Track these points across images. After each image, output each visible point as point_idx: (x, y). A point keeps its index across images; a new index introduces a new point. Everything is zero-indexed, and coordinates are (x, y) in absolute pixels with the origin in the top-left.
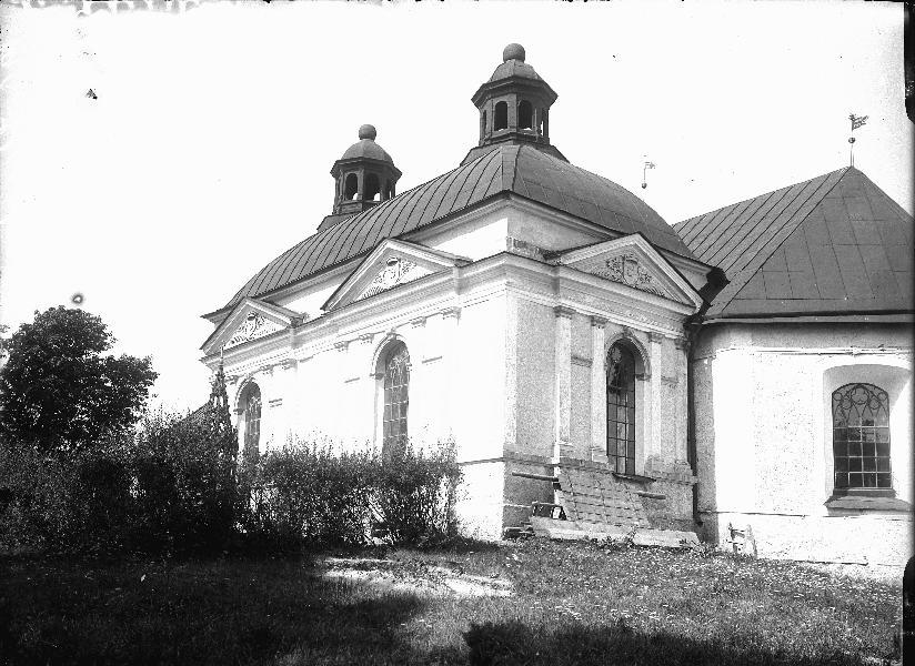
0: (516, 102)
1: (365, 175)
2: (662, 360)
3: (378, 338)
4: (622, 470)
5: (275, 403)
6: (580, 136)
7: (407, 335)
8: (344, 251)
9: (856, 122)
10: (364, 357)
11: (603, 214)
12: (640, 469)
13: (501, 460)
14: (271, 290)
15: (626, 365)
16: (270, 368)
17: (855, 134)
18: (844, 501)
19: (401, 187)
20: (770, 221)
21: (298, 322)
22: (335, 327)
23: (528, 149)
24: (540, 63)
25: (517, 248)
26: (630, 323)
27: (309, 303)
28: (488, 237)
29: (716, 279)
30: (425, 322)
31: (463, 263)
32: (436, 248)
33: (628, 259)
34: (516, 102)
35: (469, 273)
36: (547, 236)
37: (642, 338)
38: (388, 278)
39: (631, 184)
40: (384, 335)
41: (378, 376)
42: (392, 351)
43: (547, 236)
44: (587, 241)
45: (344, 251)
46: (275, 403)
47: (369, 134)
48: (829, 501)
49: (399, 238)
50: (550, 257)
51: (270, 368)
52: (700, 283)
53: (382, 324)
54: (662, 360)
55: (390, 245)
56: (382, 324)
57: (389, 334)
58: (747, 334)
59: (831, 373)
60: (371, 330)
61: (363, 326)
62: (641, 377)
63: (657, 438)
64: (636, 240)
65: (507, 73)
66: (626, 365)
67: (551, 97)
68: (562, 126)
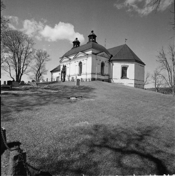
2: (106, 64)
3: (79, 61)
5: (68, 68)
6: (100, 41)
7: (82, 62)
8: (87, 48)
10: (77, 64)
11: (102, 50)
12: (104, 75)
15: (103, 65)
16: (83, 60)
19: (80, 45)
23: (94, 43)
24: (95, 33)
27: (72, 57)
28: (90, 52)
29: (112, 56)
31: (87, 55)
33: (103, 54)
34: (93, 37)
36: (96, 52)
38: (80, 56)
39: (104, 46)
42: (80, 64)
45: (87, 48)
46: (68, 68)
47: (77, 39)
49: (81, 51)
50: (96, 54)
51: (67, 64)
53: (81, 60)
55: (80, 52)
56: (79, 61)
59: (121, 66)
61: (78, 60)
63: (106, 72)
64: (104, 53)
65: (76, 41)
66: (103, 65)
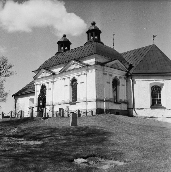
0: (94, 33)
1: (64, 44)
2: (122, 82)
3: (71, 78)
4: (115, 102)
6: (106, 40)
9: (154, 36)
10: (68, 82)
12: (118, 101)
13: (69, 103)
14: (47, 67)
15: (115, 83)
17: (154, 38)
18: (153, 106)
19: (72, 47)
20: (137, 61)
21: (54, 74)
22: (62, 76)
24: (98, 26)
25: (97, 63)
26: (116, 75)
27: (57, 70)
30: (80, 76)
31: (87, 65)
32: (83, 62)
35: (88, 67)
36: (102, 60)
37: (118, 77)
38: (72, 67)
40: (72, 77)
41: (71, 85)
42: (74, 82)
43: (102, 60)
44: (109, 60)
48: (151, 106)
50: (103, 64)
51: (48, 83)
52: (128, 67)
54: (122, 82)
57: (73, 77)
58: (102, 102)
59: (150, 84)
60: (70, 76)
61: (68, 76)
62: (118, 85)
66: (115, 83)
67: (101, 32)
68: (103, 39)
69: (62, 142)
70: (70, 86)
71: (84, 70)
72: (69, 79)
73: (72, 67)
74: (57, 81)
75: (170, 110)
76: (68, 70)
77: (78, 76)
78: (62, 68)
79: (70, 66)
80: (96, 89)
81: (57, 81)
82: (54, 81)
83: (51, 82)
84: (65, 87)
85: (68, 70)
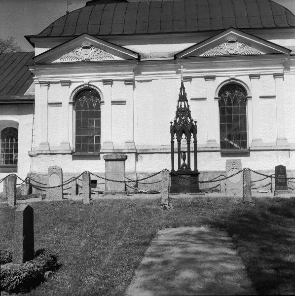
3: (74, 86)
13: (71, 154)
38: (226, 48)
41: (73, 104)
69: (232, 267)
70: (71, 106)
71: (129, 70)
72: (210, 82)
73: (226, 48)
74: (151, 81)
75: (135, 169)
76: (208, 53)
77: (251, 76)
78: (196, 43)
79: (62, 53)
80: (222, 119)
81: (151, 81)
82: (136, 79)
83: (125, 81)
84: (53, 109)
85: (208, 53)
